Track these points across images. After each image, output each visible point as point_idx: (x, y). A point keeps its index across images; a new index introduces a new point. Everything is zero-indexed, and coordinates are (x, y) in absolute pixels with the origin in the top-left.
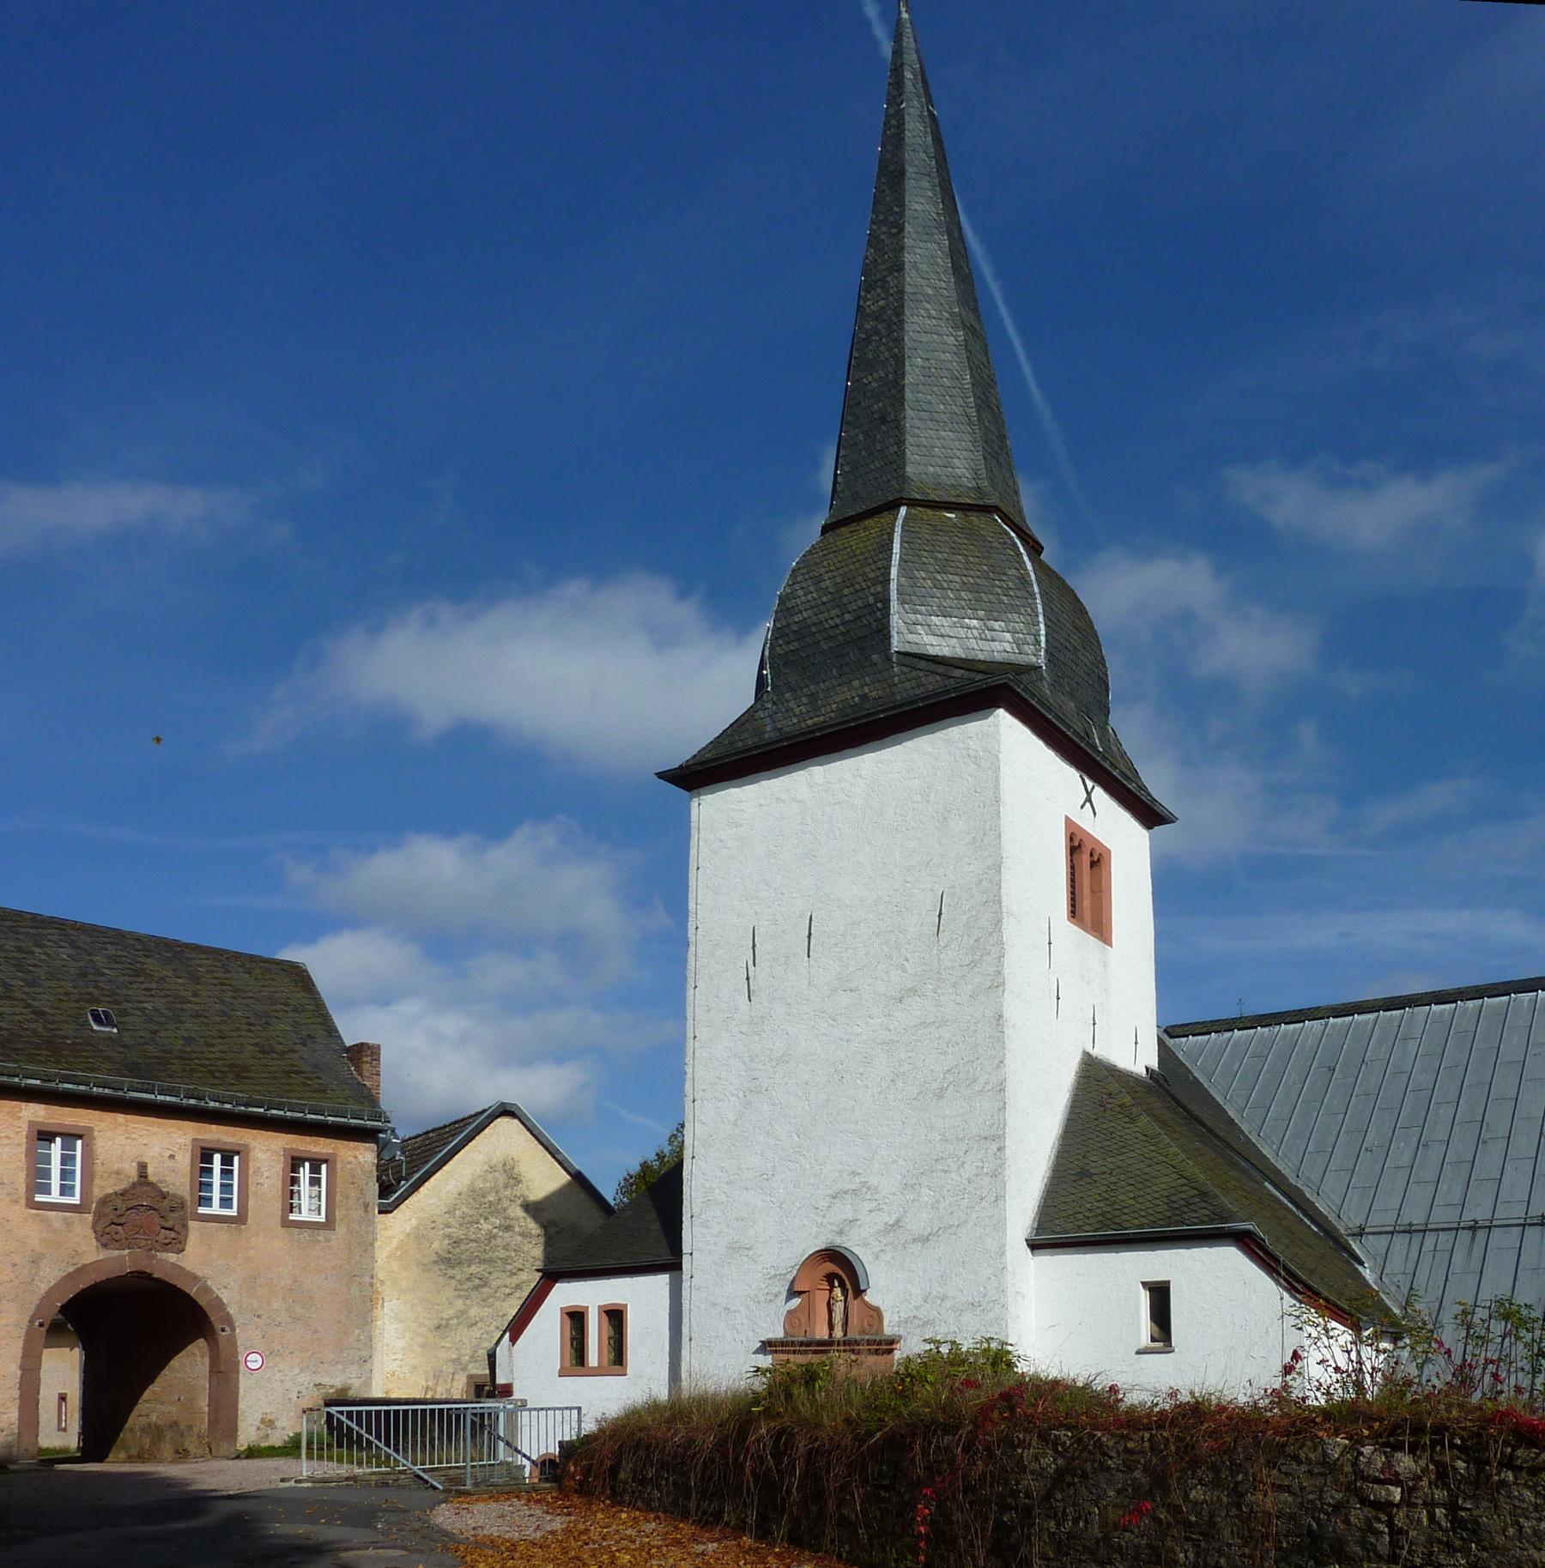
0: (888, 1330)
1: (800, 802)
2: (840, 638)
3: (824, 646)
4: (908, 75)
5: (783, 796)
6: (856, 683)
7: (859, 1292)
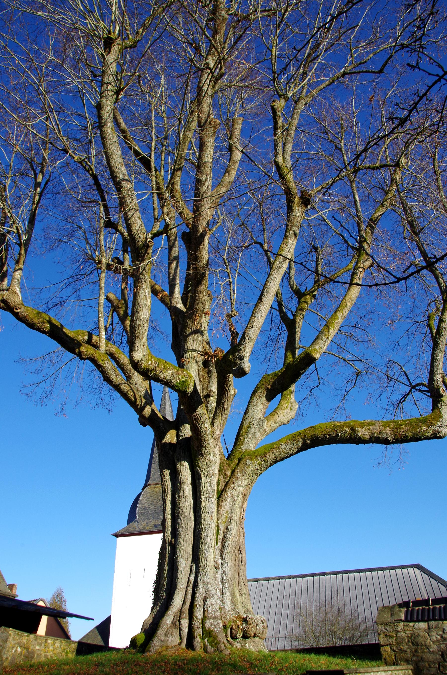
3: (150, 512)
4: (167, 396)
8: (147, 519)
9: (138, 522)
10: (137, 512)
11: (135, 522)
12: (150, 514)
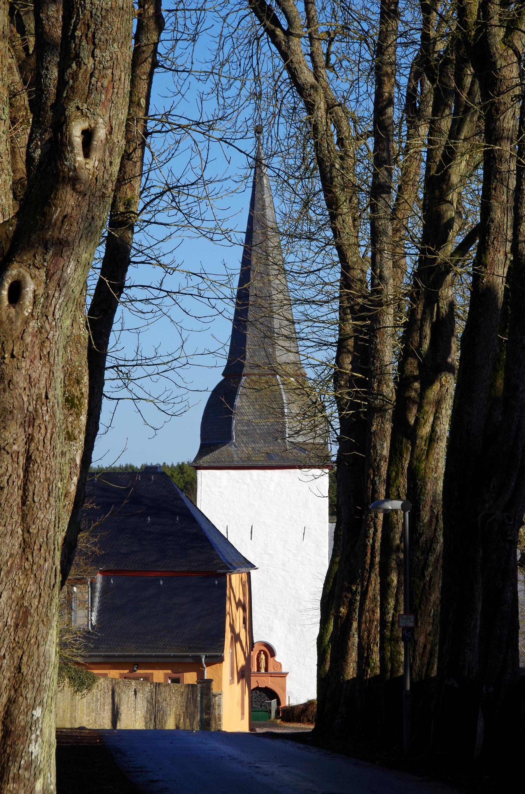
0: (284, 670)
1: (245, 483)
2: (265, 430)
5: (240, 481)
6: (271, 448)
7: (273, 654)
8: (253, 442)
9: (235, 446)
10: (233, 427)
11: (230, 446)
12: (258, 434)
